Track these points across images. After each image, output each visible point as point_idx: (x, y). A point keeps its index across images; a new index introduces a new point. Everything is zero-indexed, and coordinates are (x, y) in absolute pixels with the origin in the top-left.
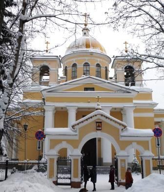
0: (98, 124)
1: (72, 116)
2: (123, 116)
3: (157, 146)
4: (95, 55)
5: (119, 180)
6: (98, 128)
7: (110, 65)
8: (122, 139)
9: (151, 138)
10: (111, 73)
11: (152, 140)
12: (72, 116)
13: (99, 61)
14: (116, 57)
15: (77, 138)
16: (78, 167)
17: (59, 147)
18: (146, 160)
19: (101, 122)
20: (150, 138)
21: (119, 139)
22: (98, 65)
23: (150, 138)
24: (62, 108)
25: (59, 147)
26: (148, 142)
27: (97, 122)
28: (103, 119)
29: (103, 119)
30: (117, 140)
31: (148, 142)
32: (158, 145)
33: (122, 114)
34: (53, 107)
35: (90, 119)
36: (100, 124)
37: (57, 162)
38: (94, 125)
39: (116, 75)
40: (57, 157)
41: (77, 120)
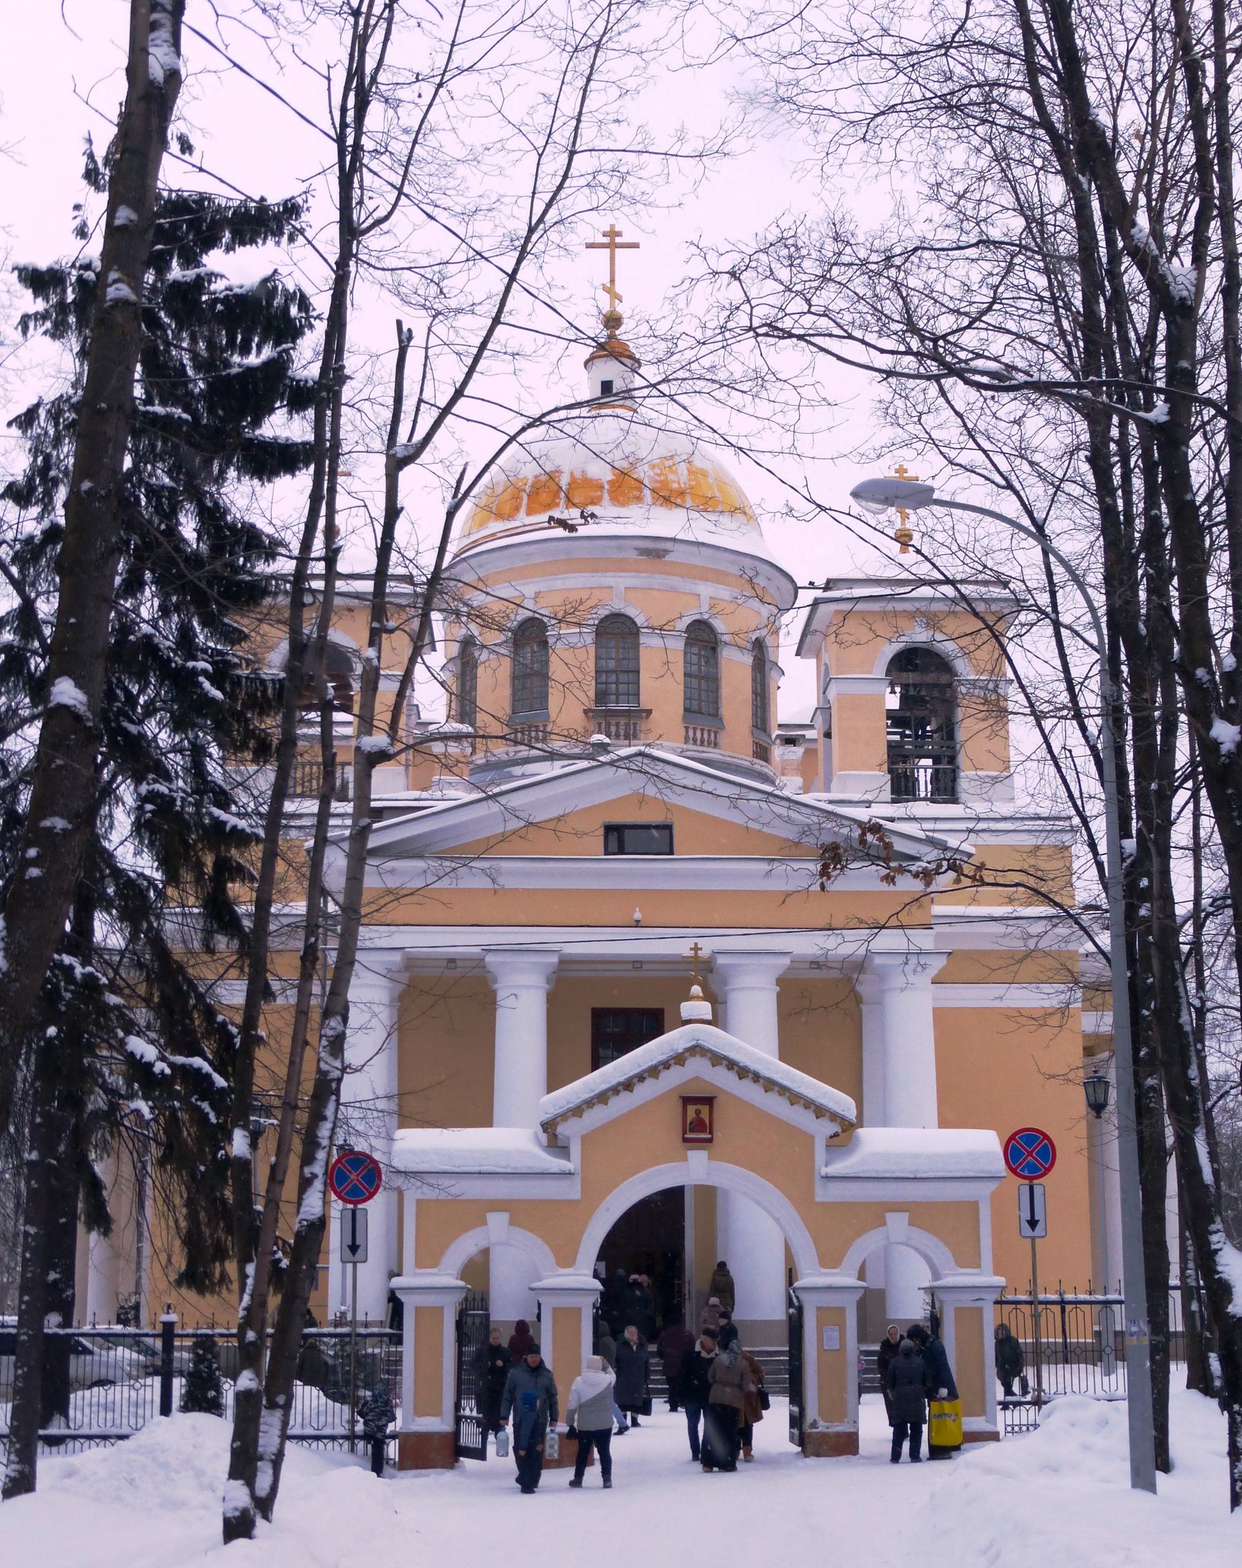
0: (691, 1109)
1: (522, 1029)
2: (864, 1008)
3: (1027, 1229)
4: (677, 555)
5: (809, 1418)
6: (688, 1136)
7: (793, 623)
8: (825, 1194)
9: (992, 1186)
10: (796, 695)
11: (994, 1196)
12: (522, 1029)
13: (705, 597)
14: (830, 585)
15: (572, 1191)
16: (982, 1344)
17: (466, 1246)
18: (958, 1310)
19: (709, 1101)
20: (983, 1191)
21: (810, 1191)
22: (702, 638)
23: (988, 1188)
24: (452, 961)
25: (466, 1246)
26: (974, 1206)
27: (687, 1101)
28: (724, 1080)
29: (724, 1080)
30: (803, 1200)
31: (974, 1206)
32: (1033, 1223)
33: (858, 1000)
34: (397, 957)
35: (650, 1082)
36: (705, 1109)
37: (459, 1325)
38: (671, 1116)
39: (824, 709)
40: (460, 1296)
41: (553, 1084)
